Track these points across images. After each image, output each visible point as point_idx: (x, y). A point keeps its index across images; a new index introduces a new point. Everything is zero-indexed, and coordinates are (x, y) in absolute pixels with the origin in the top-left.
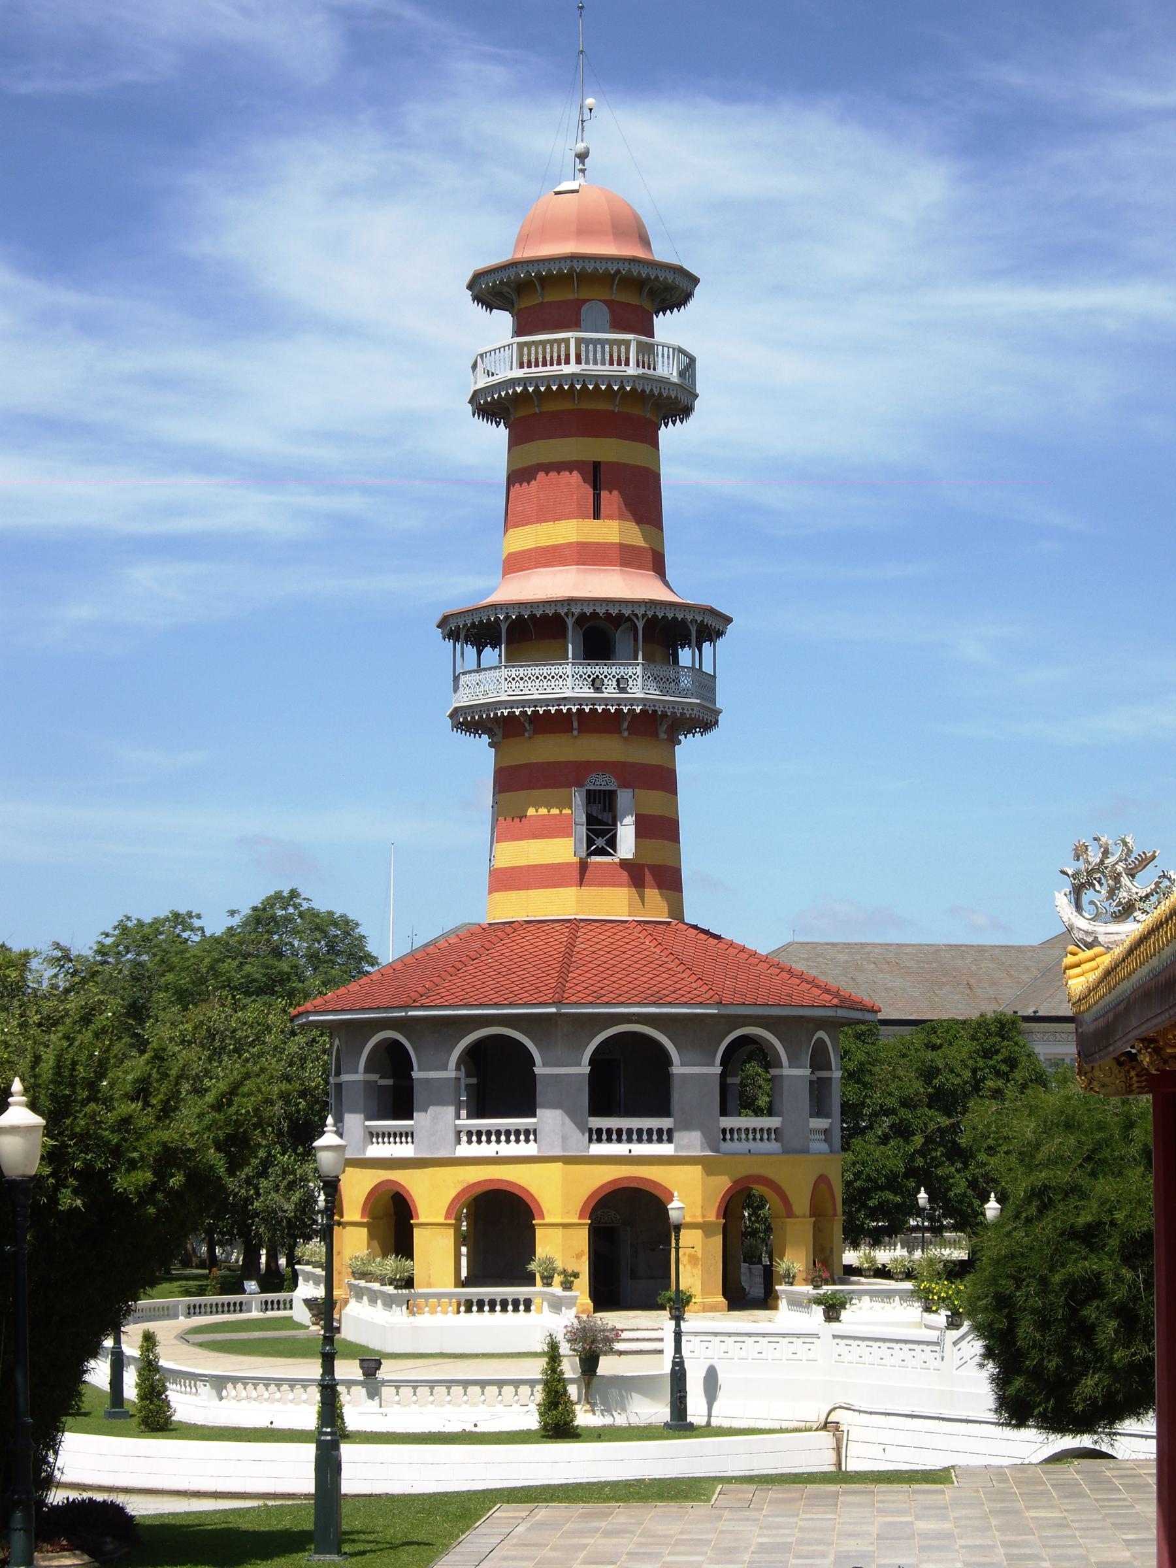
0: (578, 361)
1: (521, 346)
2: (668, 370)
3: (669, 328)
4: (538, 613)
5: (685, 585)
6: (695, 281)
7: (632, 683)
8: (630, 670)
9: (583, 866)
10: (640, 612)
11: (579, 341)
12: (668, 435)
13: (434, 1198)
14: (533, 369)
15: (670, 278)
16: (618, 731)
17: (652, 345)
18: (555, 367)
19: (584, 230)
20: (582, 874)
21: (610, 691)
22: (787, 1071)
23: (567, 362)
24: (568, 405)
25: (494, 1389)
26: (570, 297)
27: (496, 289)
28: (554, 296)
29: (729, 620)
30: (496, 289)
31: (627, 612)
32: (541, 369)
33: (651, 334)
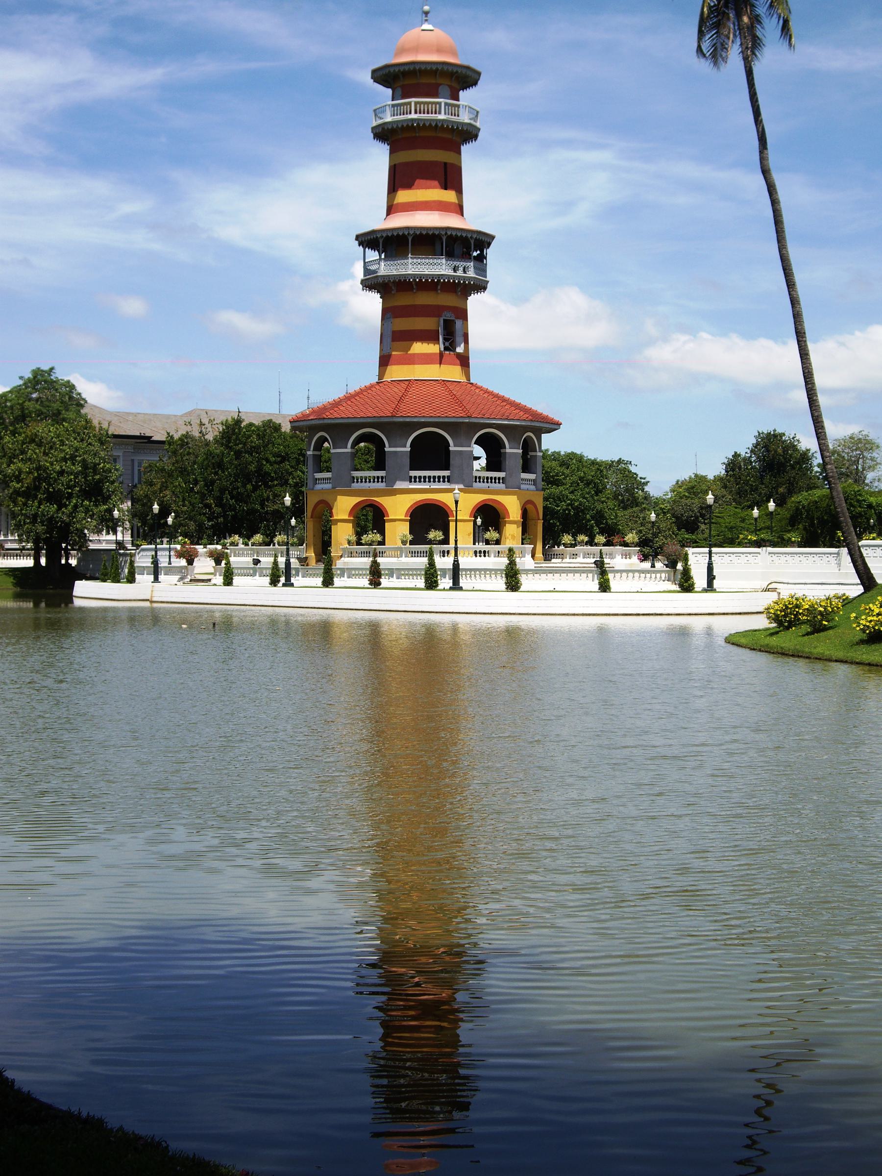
0: (416, 113)
1: (393, 106)
2: (465, 118)
3: (466, 97)
4: (431, 233)
5: (472, 220)
6: (479, 74)
7: (439, 267)
8: (468, 264)
9: (441, 355)
10: (411, 232)
11: (416, 103)
12: (465, 149)
13: (398, 508)
14: (422, 115)
15: (464, 71)
16: (455, 292)
17: (458, 106)
18: (433, 115)
19: (439, 50)
20: (440, 359)
21: (460, 273)
22: (508, 450)
23: (440, 113)
24: (448, 136)
25: (637, 574)
26: (433, 81)
27: (386, 76)
28: (424, 80)
29: (493, 237)
30: (386, 76)
31: (437, 233)
32: (426, 115)
33: (458, 100)
